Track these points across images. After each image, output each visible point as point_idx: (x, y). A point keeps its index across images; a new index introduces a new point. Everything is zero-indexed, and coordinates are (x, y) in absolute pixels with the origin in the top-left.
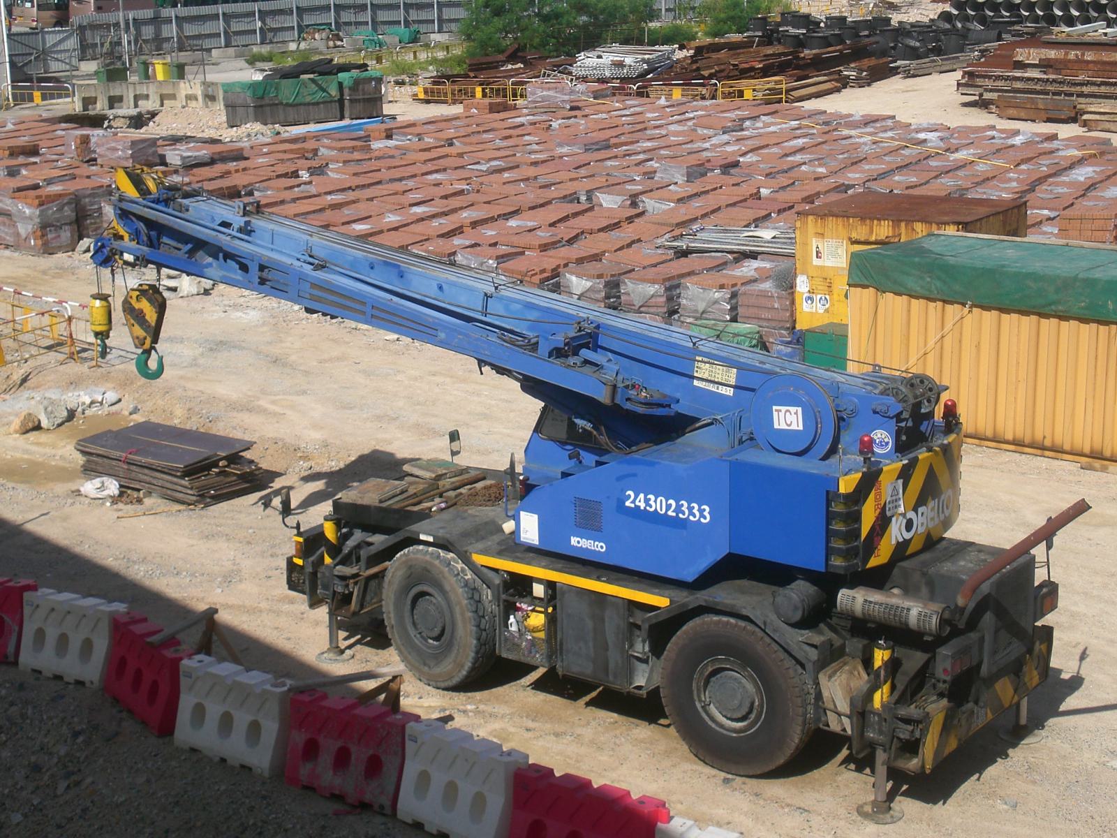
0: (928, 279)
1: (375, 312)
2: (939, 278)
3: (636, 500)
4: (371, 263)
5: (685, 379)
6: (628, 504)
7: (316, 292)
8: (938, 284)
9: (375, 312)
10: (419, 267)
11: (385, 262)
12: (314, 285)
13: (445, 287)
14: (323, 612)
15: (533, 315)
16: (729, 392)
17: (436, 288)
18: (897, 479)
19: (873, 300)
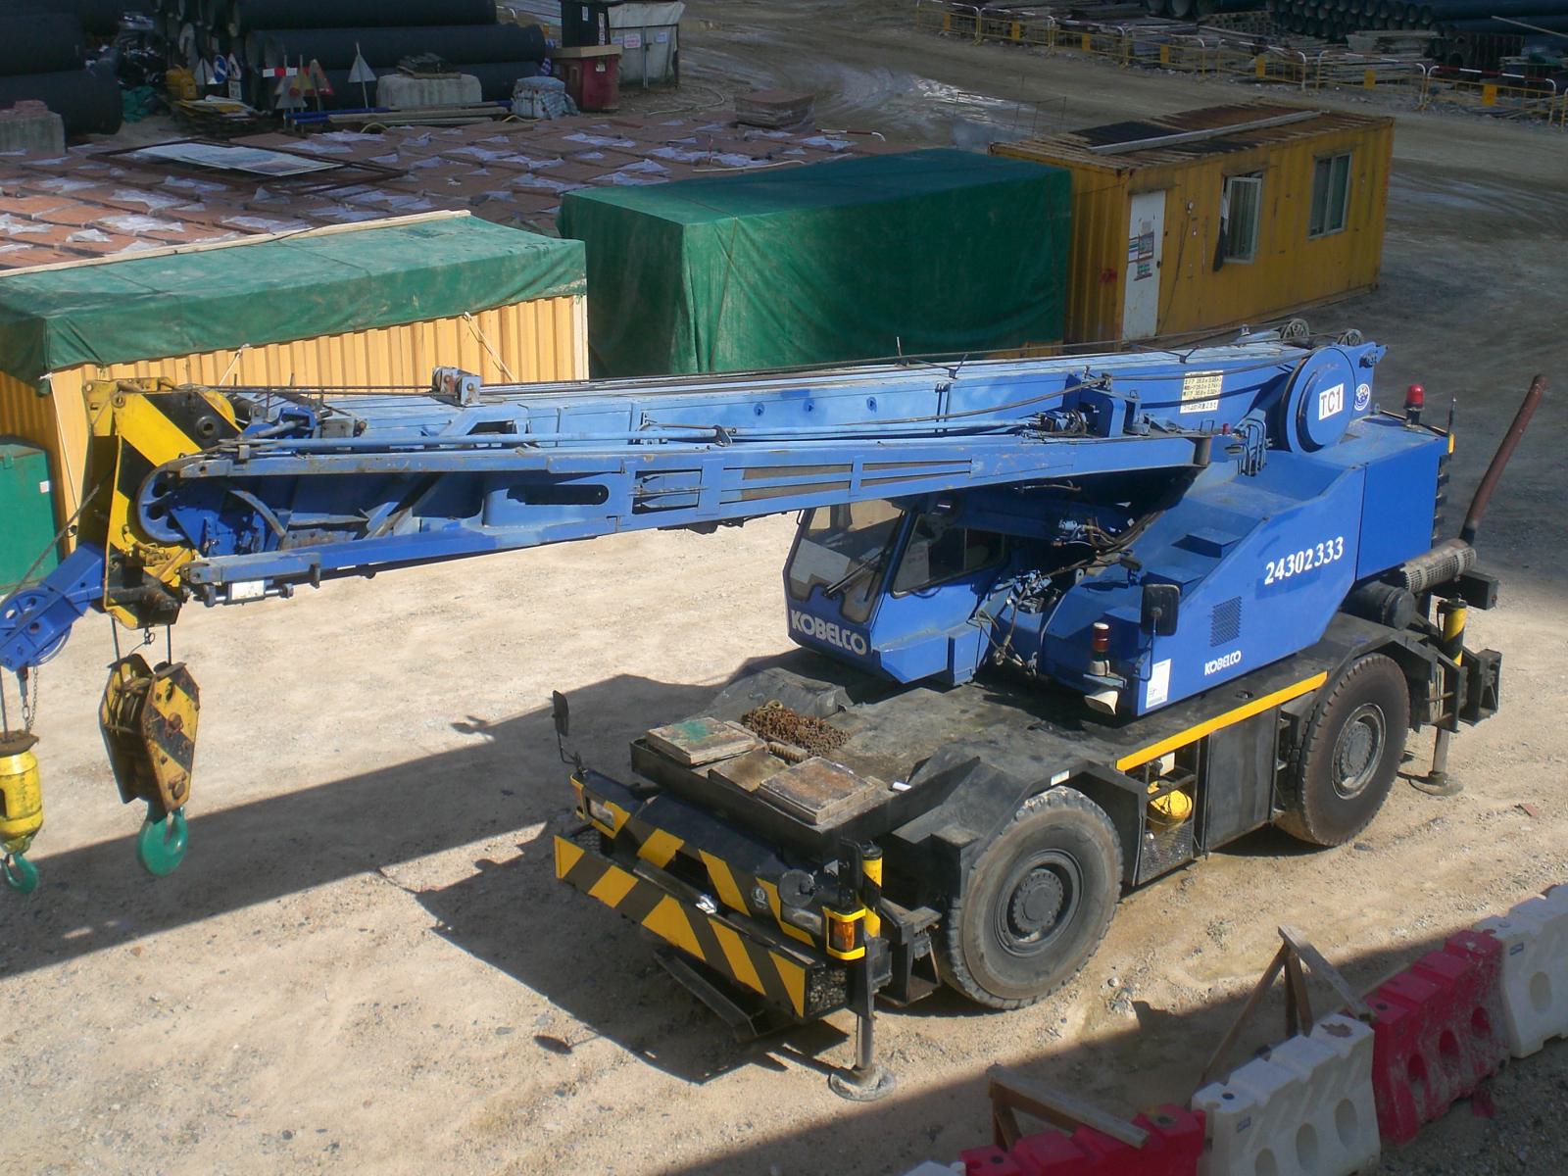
0: (177, 329)
1: (846, 476)
2: (193, 324)
3: (1276, 571)
4: (760, 404)
5: (1172, 409)
6: (1340, 539)
7: (755, 483)
8: (193, 331)
9: (846, 476)
10: (831, 383)
11: (782, 393)
12: (750, 471)
13: (879, 400)
14: (1461, 725)
15: (999, 398)
16: (1212, 406)
17: (864, 404)
18: (383, 875)
19: (464, 362)
